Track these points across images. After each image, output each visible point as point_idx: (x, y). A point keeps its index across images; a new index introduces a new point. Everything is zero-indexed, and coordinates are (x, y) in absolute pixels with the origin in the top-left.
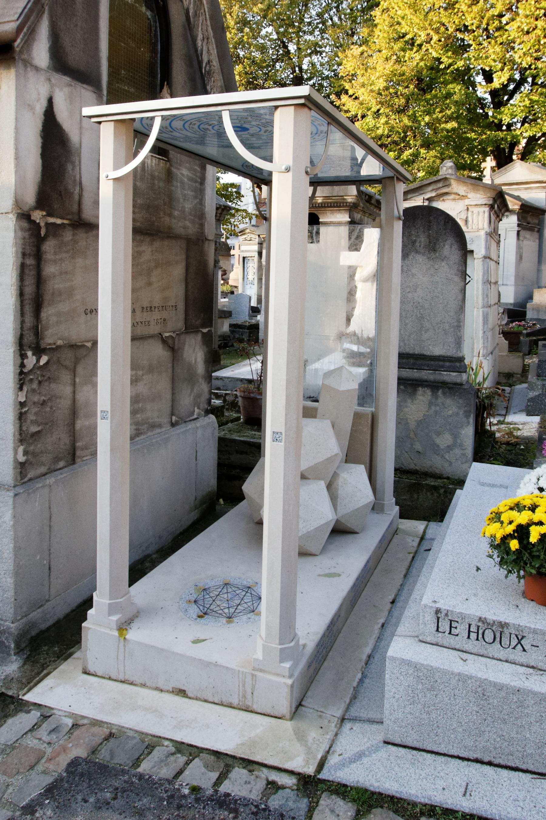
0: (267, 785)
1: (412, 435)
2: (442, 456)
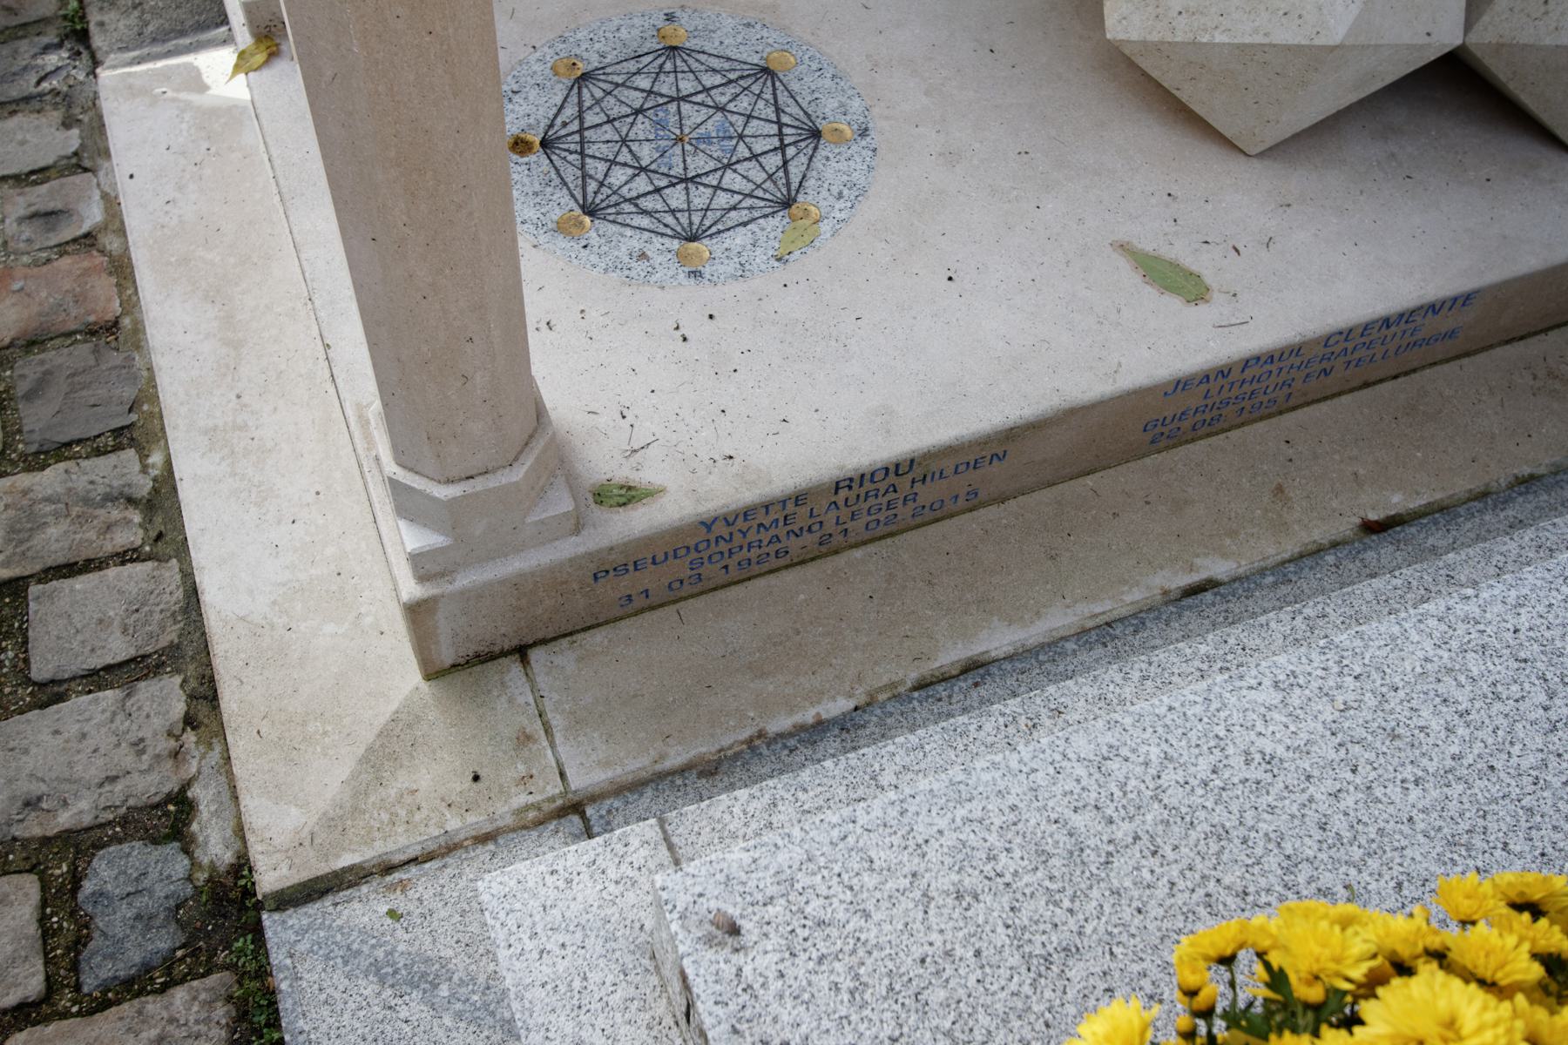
0: (169, 798)
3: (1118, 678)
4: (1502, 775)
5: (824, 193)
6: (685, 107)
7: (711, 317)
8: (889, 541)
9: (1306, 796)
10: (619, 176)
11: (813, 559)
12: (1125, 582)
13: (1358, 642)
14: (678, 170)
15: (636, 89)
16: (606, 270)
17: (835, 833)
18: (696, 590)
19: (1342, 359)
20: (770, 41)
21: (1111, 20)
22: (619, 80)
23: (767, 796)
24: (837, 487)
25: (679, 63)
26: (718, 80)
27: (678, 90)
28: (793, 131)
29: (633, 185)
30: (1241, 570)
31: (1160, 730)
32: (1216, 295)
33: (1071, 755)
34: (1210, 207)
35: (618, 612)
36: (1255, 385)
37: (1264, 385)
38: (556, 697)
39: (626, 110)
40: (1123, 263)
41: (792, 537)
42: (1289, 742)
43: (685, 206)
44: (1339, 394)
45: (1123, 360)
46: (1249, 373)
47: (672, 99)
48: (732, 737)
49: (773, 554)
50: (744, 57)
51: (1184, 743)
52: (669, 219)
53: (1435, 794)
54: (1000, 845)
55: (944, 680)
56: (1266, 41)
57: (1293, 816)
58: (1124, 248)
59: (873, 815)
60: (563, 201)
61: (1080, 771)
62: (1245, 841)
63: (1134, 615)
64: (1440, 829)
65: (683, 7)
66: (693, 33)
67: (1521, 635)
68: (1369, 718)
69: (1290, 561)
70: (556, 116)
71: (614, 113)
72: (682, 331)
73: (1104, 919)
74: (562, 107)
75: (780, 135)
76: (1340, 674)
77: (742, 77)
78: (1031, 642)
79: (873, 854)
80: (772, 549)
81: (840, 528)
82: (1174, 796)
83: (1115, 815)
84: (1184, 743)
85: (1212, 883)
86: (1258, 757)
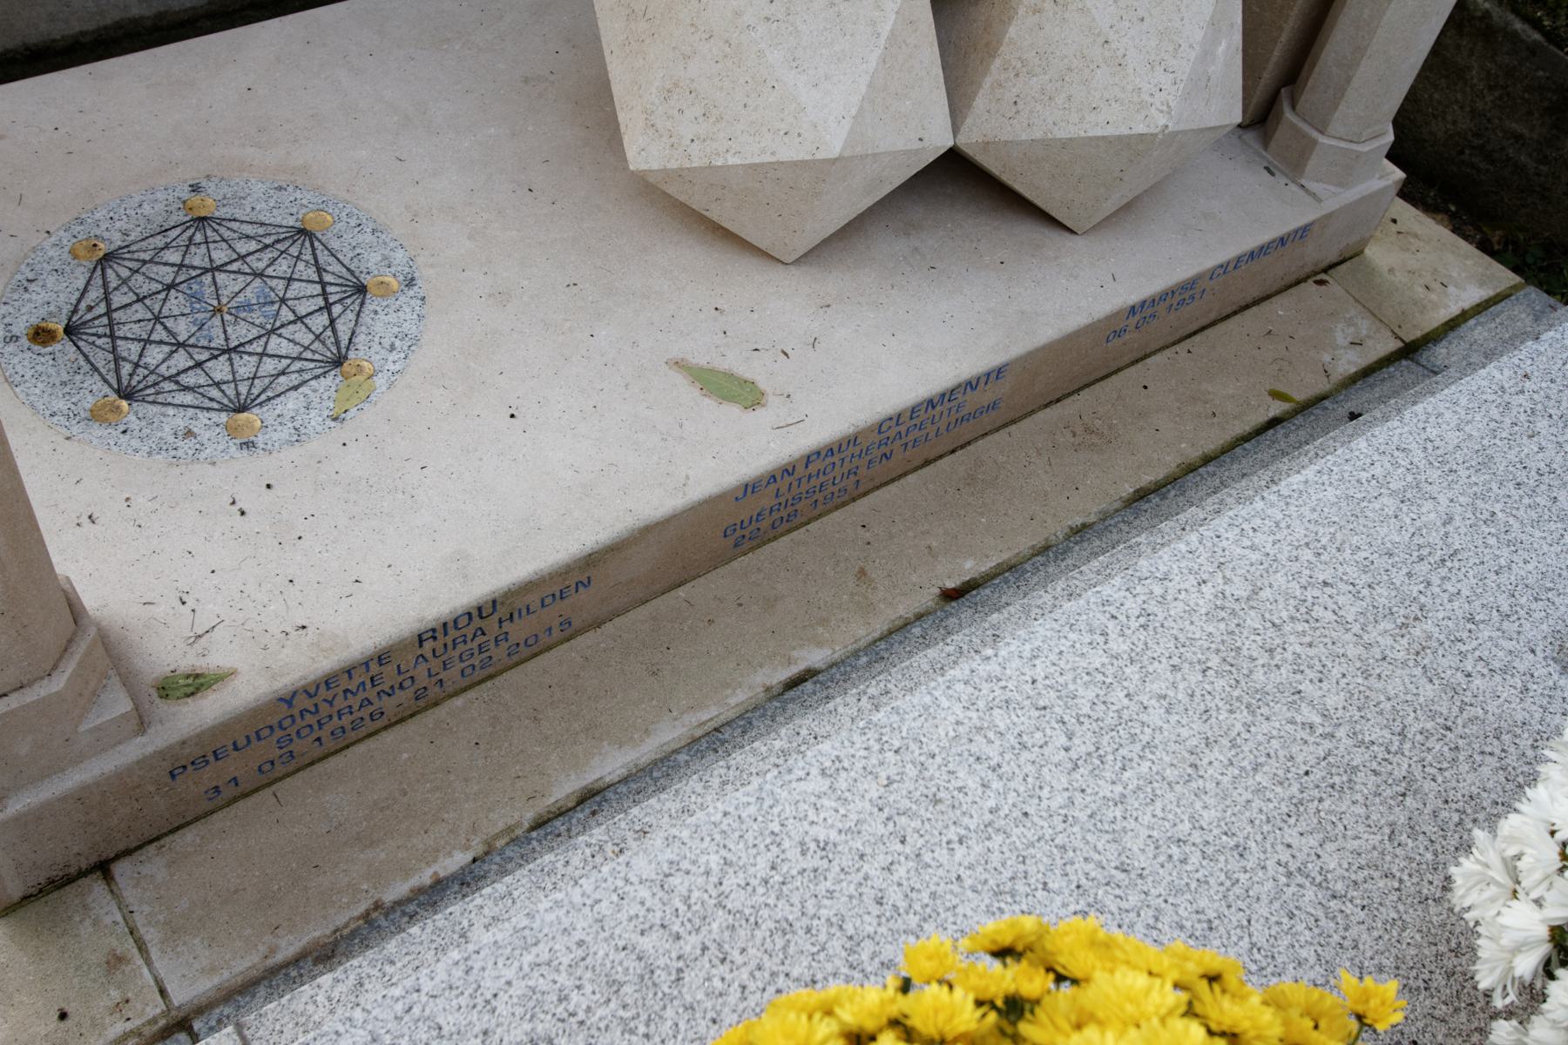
3: (699, 788)
4: (1036, 819)
5: (376, 347)
6: (221, 278)
7: (269, 486)
8: (489, 684)
9: (861, 875)
10: (154, 355)
11: (412, 716)
12: (728, 686)
13: (895, 718)
14: (219, 342)
15: (166, 264)
16: (150, 454)
17: (399, 1007)
18: (291, 768)
19: (898, 442)
20: (305, 202)
21: (631, 152)
22: (147, 256)
23: (352, 977)
24: (421, 640)
25: (209, 233)
26: (253, 246)
27: (211, 260)
28: (338, 289)
29: (172, 362)
31: (718, 837)
32: (771, 398)
33: (634, 879)
34: (755, 315)
35: (206, 806)
36: (822, 478)
38: (147, 909)
39: (156, 287)
40: (679, 379)
41: (384, 697)
42: (840, 825)
43: (230, 377)
44: (905, 474)
45: (691, 473)
46: (813, 468)
47: (206, 271)
48: (346, 914)
49: (367, 718)
50: (278, 221)
51: (741, 845)
52: (214, 393)
53: (978, 849)
54: (569, 983)
55: (561, 814)
56: (773, 159)
57: (851, 897)
58: (679, 365)
59: (438, 979)
60: (95, 387)
61: (644, 893)
62: (808, 930)
63: (741, 717)
64: (986, 881)
65: (208, 177)
66: (222, 202)
67: (1039, 685)
69: (880, 639)
70: (79, 301)
71: (144, 291)
72: (239, 505)
73: (680, 1037)
74: (85, 291)
75: (324, 294)
76: (881, 751)
77: (278, 241)
78: (644, 761)
79: (441, 1020)
80: (365, 713)
81: (434, 680)
82: (737, 900)
83: (681, 930)
84: (741, 845)
85: (782, 977)
86: (813, 846)
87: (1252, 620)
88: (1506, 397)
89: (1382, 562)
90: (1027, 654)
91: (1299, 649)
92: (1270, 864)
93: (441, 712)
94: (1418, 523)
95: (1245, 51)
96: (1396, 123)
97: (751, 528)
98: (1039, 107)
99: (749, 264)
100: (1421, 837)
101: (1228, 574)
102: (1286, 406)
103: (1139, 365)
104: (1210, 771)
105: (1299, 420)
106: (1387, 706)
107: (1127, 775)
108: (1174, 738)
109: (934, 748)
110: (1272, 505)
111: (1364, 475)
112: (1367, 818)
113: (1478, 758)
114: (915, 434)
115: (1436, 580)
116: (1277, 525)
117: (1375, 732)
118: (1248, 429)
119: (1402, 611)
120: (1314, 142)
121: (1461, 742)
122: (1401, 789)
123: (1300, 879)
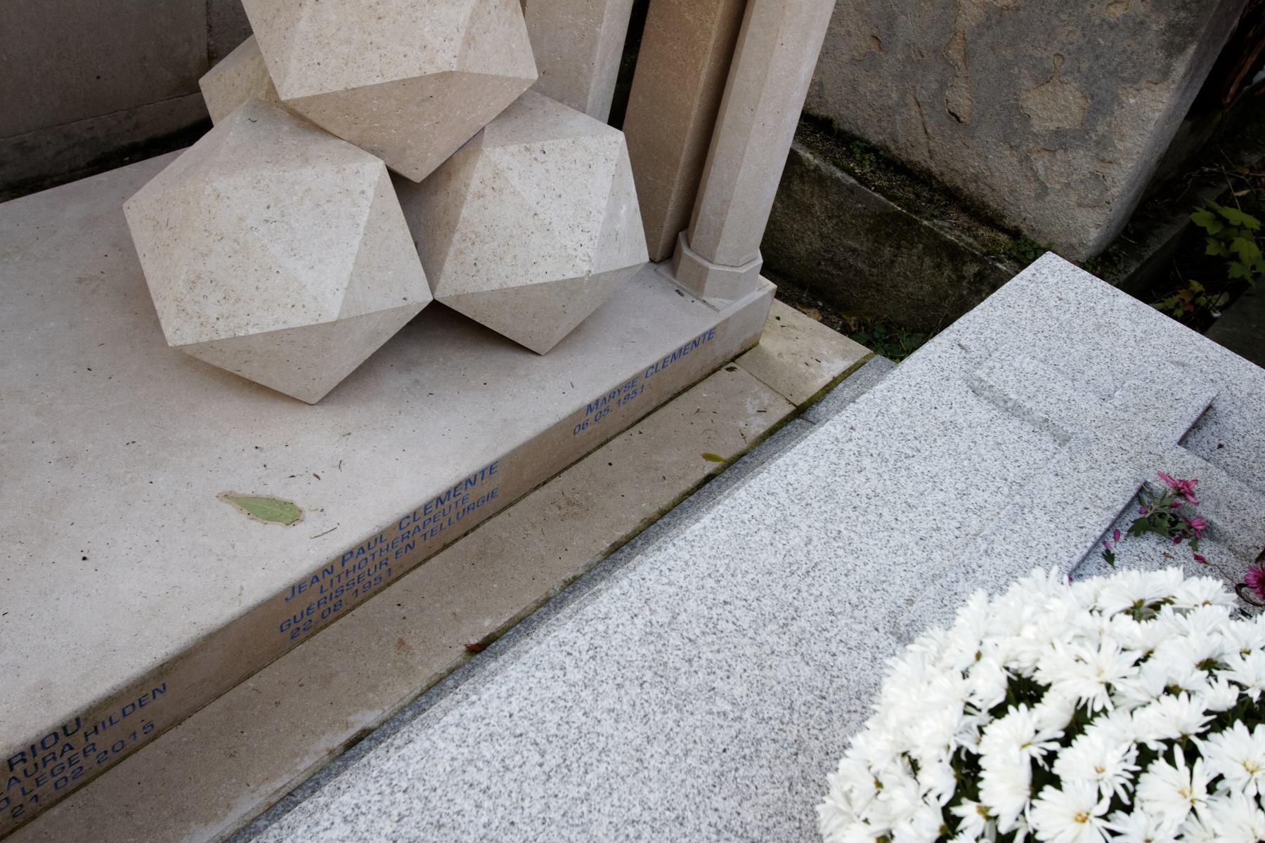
1: (955, 54)
2: (1025, 159)
4: (521, 826)
8: (83, 791)
11: (12, 832)
12: (297, 755)
13: (401, 764)
19: (418, 535)
30: (386, 714)
32: (307, 514)
34: (290, 449)
36: (358, 572)
37: (365, 569)
40: (229, 509)
44: (429, 558)
45: (244, 584)
56: (286, 327)
58: (228, 497)
63: (310, 779)
67: (515, 717)
68: (419, 819)
76: (392, 793)
78: (228, 832)
81: (28, 797)
87: (674, 639)
88: (840, 445)
89: (764, 580)
90: (504, 694)
91: (710, 656)
92: (704, 827)
93: (39, 824)
94: (788, 547)
95: (641, 210)
96: (764, 248)
97: (303, 621)
98: (493, 266)
99: (285, 407)
100: (812, 784)
101: (653, 606)
102: (717, 465)
103: (604, 448)
104: (653, 762)
105: (727, 474)
106: (778, 688)
107: (589, 777)
108: (622, 741)
109: (435, 783)
110: (681, 549)
111: (746, 517)
112: (772, 776)
113: (846, 716)
114: (432, 525)
115: (804, 587)
116: (686, 563)
117: (772, 710)
118: (690, 486)
119: (783, 615)
120: (707, 269)
121: (833, 707)
122: (794, 750)
123: (726, 834)
